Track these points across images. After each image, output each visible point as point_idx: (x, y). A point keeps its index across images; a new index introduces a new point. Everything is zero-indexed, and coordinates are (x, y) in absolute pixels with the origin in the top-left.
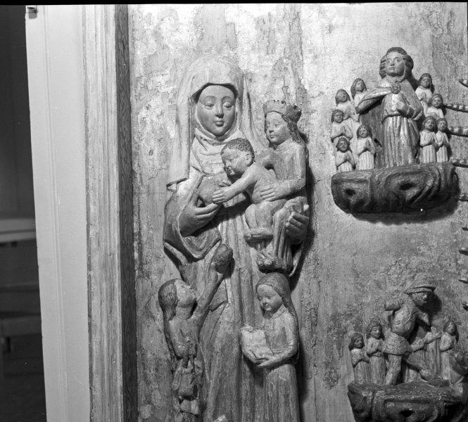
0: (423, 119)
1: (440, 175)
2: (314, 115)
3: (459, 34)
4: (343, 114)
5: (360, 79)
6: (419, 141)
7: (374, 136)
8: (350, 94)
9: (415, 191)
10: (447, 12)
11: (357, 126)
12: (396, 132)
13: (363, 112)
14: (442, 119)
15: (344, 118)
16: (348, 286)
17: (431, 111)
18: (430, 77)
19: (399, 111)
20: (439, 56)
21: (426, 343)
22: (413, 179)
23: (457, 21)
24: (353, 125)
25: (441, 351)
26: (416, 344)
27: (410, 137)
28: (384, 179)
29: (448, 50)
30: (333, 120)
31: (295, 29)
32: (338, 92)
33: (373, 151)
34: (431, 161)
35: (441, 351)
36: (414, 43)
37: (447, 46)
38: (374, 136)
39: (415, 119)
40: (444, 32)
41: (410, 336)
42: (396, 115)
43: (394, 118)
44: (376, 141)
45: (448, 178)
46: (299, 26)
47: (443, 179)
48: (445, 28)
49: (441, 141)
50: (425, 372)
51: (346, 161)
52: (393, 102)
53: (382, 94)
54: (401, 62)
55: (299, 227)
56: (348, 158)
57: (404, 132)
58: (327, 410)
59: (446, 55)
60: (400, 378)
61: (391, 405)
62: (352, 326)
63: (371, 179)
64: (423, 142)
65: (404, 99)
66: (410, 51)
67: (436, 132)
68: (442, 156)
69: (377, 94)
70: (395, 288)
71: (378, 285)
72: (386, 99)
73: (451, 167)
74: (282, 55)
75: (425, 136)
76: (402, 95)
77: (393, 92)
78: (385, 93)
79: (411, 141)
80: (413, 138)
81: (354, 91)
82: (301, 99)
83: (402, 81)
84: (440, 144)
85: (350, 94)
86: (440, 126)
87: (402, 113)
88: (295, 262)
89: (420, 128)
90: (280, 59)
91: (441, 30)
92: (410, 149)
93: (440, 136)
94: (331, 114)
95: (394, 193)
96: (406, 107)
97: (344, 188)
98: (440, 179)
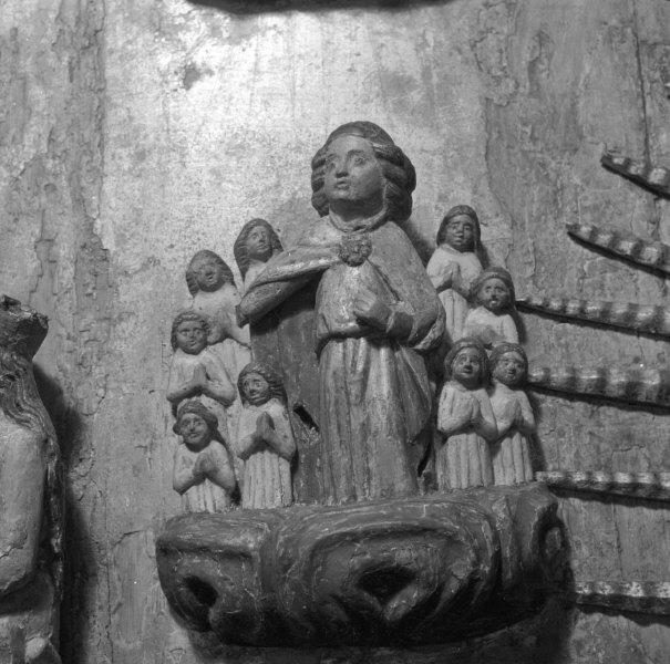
0: (443, 345)
1: (496, 539)
2: (126, 327)
3: (564, 96)
4: (205, 327)
5: (259, 222)
6: (434, 417)
7: (293, 398)
8: (234, 267)
9: (410, 597)
10: (529, 35)
11: (244, 358)
12: (354, 390)
13: (263, 321)
14: (510, 347)
15: (211, 339)
17: (467, 323)
18: (473, 215)
19: (361, 320)
20: (504, 157)
22: (403, 553)
23: (557, 57)
24: (233, 358)
27: (402, 406)
29: (533, 139)
30: (176, 344)
31: (87, 75)
32: (344, 129)
34: (475, 481)
36: (425, 115)
37: (528, 130)
38: (293, 398)
39: (419, 347)
40: (521, 89)
42: (356, 335)
43: (350, 342)
44: (302, 413)
45: (528, 545)
46: (99, 68)
47: (507, 552)
48: (524, 76)
49: (506, 415)
52: (346, 294)
53: (312, 264)
54: (369, 166)
56: (208, 466)
57: (380, 385)
59: (525, 153)
63: (262, 549)
64: (446, 420)
65: (382, 284)
66: (406, 138)
67: (490, 388)
68: (511, 467)
69: (298, 267)
72: (328, 281)
73: (539, 505)
74: (44, 148)
75: (453, 402)
76: (376, 268)
77: (345, 261)
78: (322, 262)
79: (403, 421)
80: (413, 409)
81: (244, 255)
82: (88, 278)
83: (375, 227)
84: (502, 425)
85: (234, 267)
86: (503, 368)
87: (371, 330)
89: (439, 376)
90: (38, 159)
91: (512, 84)
92: (397, 446)
93: (501, 404)
94: (169, 325)
95: (339, 600)
96: (383, 309)
97: (182, 572)
98: (498, 556)
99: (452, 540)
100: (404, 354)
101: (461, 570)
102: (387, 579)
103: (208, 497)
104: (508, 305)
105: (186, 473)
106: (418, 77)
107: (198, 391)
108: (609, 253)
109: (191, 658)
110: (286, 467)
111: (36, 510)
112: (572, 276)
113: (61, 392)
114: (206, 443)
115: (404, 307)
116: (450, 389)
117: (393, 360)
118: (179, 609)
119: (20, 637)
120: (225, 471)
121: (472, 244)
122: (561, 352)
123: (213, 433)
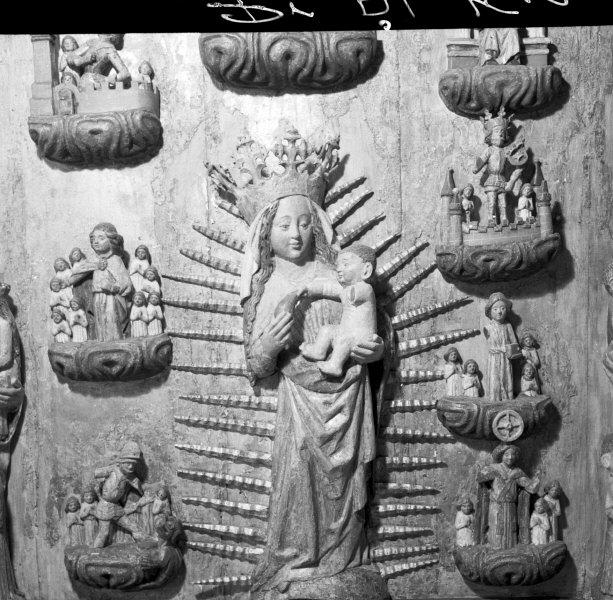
9: (115, 369)
13: (77, 284)
16: (68, 451)
21: (140, 507)
22: (114, 357)
24: (68, 294)
25: (154, 515)
26: (131, 506)
27: (117, 314)
28: (86, 356)
32: (98, 227)
33: (85, 323)
35: (154, 515)
41: (120, 502)
50: (136, 535)
51: (60, 332)
52: (100, 281)
55: (8, 400)
57: (110, 308)
58: (49, 567)
60: (107, 542)
61: (92, 569)
62: (72, 489)
64: (133, 316)
68: (155, 329)
70: (114, 454)
71: (98, 450)
75: (135, 311)
84: (151, 318)
88: (12, 430)
93: (151, 309)
99: (128, 353)
100: (118, 297)
101: (131, 361)
102: (110, 363)
103: (62, 338)
104: (157, 278)
105: (55, 331)
106: (131, 194)
107: (58, 305)
108: (193, 258)
109: (74, 595)
110: (85, 330)
111: (10, 344)
112: (181, 266)
113: (147, 393)
114: (61, 321)
115: (117, 285)
116: (134, 307)
117: (115, 300)
118: (54, 370)
119: (9, 378)
120: (68, 330)
121: (148, 257)
122: (173, 291)
123: (64, 317)
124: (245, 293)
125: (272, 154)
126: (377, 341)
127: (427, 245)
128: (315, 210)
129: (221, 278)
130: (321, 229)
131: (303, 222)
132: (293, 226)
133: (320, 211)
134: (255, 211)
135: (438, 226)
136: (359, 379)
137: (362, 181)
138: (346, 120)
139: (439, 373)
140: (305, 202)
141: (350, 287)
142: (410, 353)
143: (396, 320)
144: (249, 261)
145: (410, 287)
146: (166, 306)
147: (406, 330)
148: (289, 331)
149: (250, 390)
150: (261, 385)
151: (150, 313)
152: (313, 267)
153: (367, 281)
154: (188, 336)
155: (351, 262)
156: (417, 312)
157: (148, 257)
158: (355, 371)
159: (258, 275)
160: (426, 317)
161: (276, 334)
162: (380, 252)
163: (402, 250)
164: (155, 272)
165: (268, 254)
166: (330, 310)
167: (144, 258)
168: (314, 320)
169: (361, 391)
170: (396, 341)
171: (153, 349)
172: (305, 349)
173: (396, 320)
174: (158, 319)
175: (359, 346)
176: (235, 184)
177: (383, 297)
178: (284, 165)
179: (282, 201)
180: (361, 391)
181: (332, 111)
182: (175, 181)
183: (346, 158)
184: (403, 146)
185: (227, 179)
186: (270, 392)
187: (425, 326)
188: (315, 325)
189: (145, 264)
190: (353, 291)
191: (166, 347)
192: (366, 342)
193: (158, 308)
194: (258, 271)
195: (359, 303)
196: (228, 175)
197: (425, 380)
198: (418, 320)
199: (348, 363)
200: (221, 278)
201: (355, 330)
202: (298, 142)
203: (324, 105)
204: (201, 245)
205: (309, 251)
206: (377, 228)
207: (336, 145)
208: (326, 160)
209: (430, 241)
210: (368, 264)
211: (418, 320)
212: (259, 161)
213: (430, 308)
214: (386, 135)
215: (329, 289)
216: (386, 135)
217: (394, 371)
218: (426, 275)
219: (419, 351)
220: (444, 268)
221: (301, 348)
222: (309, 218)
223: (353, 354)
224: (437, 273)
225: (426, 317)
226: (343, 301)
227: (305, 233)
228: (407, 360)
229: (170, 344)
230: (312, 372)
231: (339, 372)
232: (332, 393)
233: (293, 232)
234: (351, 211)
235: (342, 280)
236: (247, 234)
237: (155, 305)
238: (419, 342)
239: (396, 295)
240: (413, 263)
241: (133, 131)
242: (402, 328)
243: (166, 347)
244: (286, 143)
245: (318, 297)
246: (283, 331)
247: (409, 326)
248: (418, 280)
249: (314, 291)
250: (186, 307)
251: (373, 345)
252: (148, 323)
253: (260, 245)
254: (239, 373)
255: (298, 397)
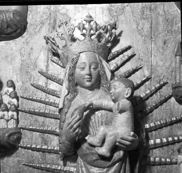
84: (9, 118)
124: (61, 106)
125: (77, 29)
126: (133, 136)
127: (167, 83)
128: (101, 61)
129: (52, 99)
130: (105, 72)
131: (92, 67)
132: (87, 68)
133: (104, 63)
134: (68, 61)
135: (173, 73)
136: (122, 160)
137: (129, 48)
138: (122, 18)
139: (174, 160)
140: (95, 56)
141: (117, 103)
142: (156, 146)
143: (147, 126)
144: (63, 90)
145: (156, 107)
146: (20, 112)
147: (154, 132)
148: (78, 126)
149: (61, 163)
150: (68, 160)
151: (9, 116)
152: (99, 93)
153: (128, 99)
154: (31, 130)
155: (119, 88)
156: (160, 122)
157: (13, 86)
158: (120, 154)
159: (68, 96)
160: (166, 125)
161: (71, 128)
162: (139, 86)
163: (152, 85)
164: (16, 94)
165: (74, 84)
166: (107, 117)
167: (11, 87)
168: (97, 123)
169: (123, 168)
170: (148, 139)
171: (6, 135)
172: (89, 139)
173: (147, 126)
174: (14, 119)
175: (121, 139)
176: (58, 47)
177: (139, 110)
178: (84, 35)
179: (81, 54)
180: (123, 168)
181: (115, 14)
182: (32, 49)
183: (120, 35)
184: (153, 29)
185: (54, 44)
186: (73, 164)
187: (165, 131)
188: (97, 126)
189: (11, 90)
190: (119, 104)
191: (17, 134)
192: (126, 136)
193: (15, 113)
194: (68, 94)
195: (121, 112)
196: (54, 42)
197: (166, 164)
198: (161, 127)
199: (114, 149)
200: (52, 99)
201: (121, 128)
202: (92, 23)
203: (110, 10)
204: (42, 81)
205: (97, 83)
206: (137, 73)
207: (114, 27)
208: (108, 34)
209: (168, 81)
210: (128, 88)
211: (161, 127)
212: (70, 33)
213: (168, 120)
214: (144, 24)
215: (106, 104)
216: (144, 24)
217: (146, 157)
218: (166, 100)
219: (162, 145)
220: (177, 96)
221: (87, 138)
222: (97, 65)
223: (117, 143)
224: (173, 99)
225: (166, 125)
226: (114, 111)
227: (94, 73)
228: (154, 150)
229: (20, 133)
230: (93, 154)
231: (108, 155)
232: (104, 168)
233: (86, 71)
234: (123, 64)
235: (113, 98)
236: (61, 73)
237: (13, 111)
238: (161, 140)
239: (148, 112)
240: (158, 93)
241: (9, 20)
242: (151, 131)
243: (17, 134)
244: (84, 22)
245: (99, 109)
246: (75, 126)
247: (155, 130)
248: (161, 103)
249: (97, 105)
250: (30, 113)
251: (131, 138)
252: (8, 121)
253: (69, 79)
254: (56, 152)
255: (84, 169)
